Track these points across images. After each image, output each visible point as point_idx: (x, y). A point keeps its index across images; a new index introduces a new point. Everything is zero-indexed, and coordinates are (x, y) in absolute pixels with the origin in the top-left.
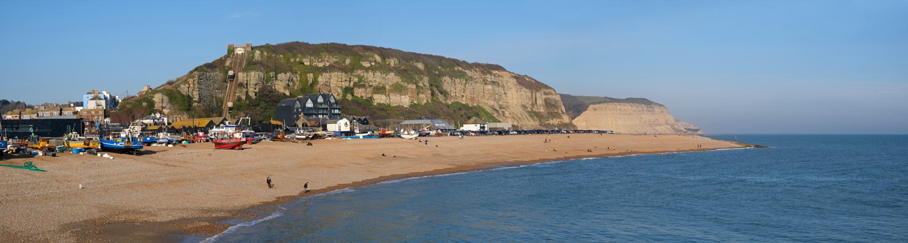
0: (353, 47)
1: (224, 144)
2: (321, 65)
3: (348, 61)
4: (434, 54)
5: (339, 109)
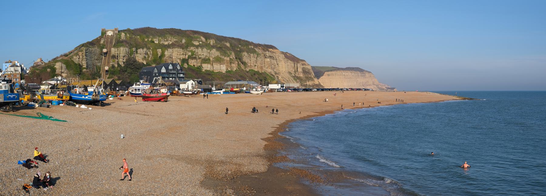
0: (186, 31)
1: (152, 97)
2: (166, 43)
4: (235, 37)
5: (183, 74)
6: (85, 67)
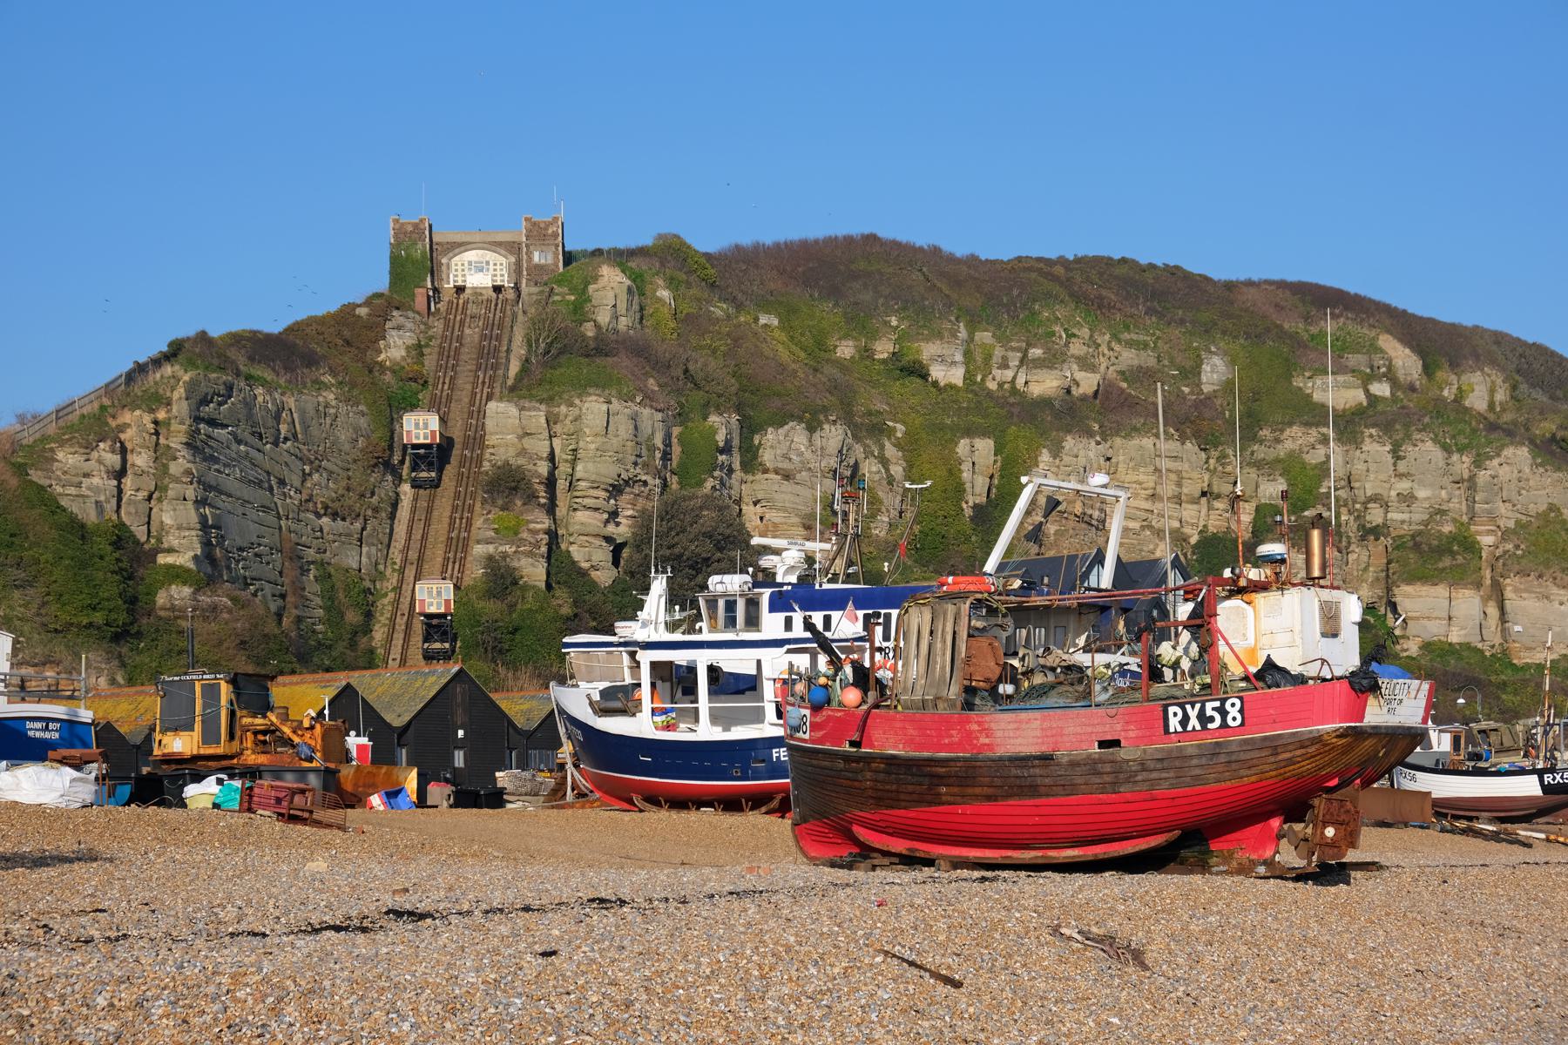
0: (1230, 286)
1: (1024, 776)
2: (1044, 384)
3: (1214, 371)
6: (184, 559)
